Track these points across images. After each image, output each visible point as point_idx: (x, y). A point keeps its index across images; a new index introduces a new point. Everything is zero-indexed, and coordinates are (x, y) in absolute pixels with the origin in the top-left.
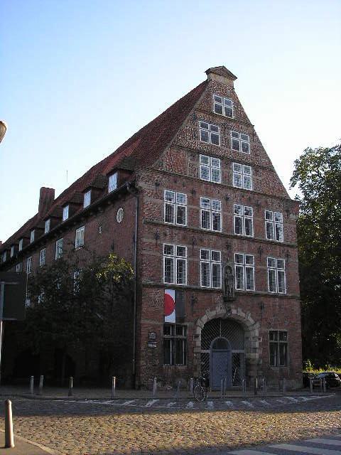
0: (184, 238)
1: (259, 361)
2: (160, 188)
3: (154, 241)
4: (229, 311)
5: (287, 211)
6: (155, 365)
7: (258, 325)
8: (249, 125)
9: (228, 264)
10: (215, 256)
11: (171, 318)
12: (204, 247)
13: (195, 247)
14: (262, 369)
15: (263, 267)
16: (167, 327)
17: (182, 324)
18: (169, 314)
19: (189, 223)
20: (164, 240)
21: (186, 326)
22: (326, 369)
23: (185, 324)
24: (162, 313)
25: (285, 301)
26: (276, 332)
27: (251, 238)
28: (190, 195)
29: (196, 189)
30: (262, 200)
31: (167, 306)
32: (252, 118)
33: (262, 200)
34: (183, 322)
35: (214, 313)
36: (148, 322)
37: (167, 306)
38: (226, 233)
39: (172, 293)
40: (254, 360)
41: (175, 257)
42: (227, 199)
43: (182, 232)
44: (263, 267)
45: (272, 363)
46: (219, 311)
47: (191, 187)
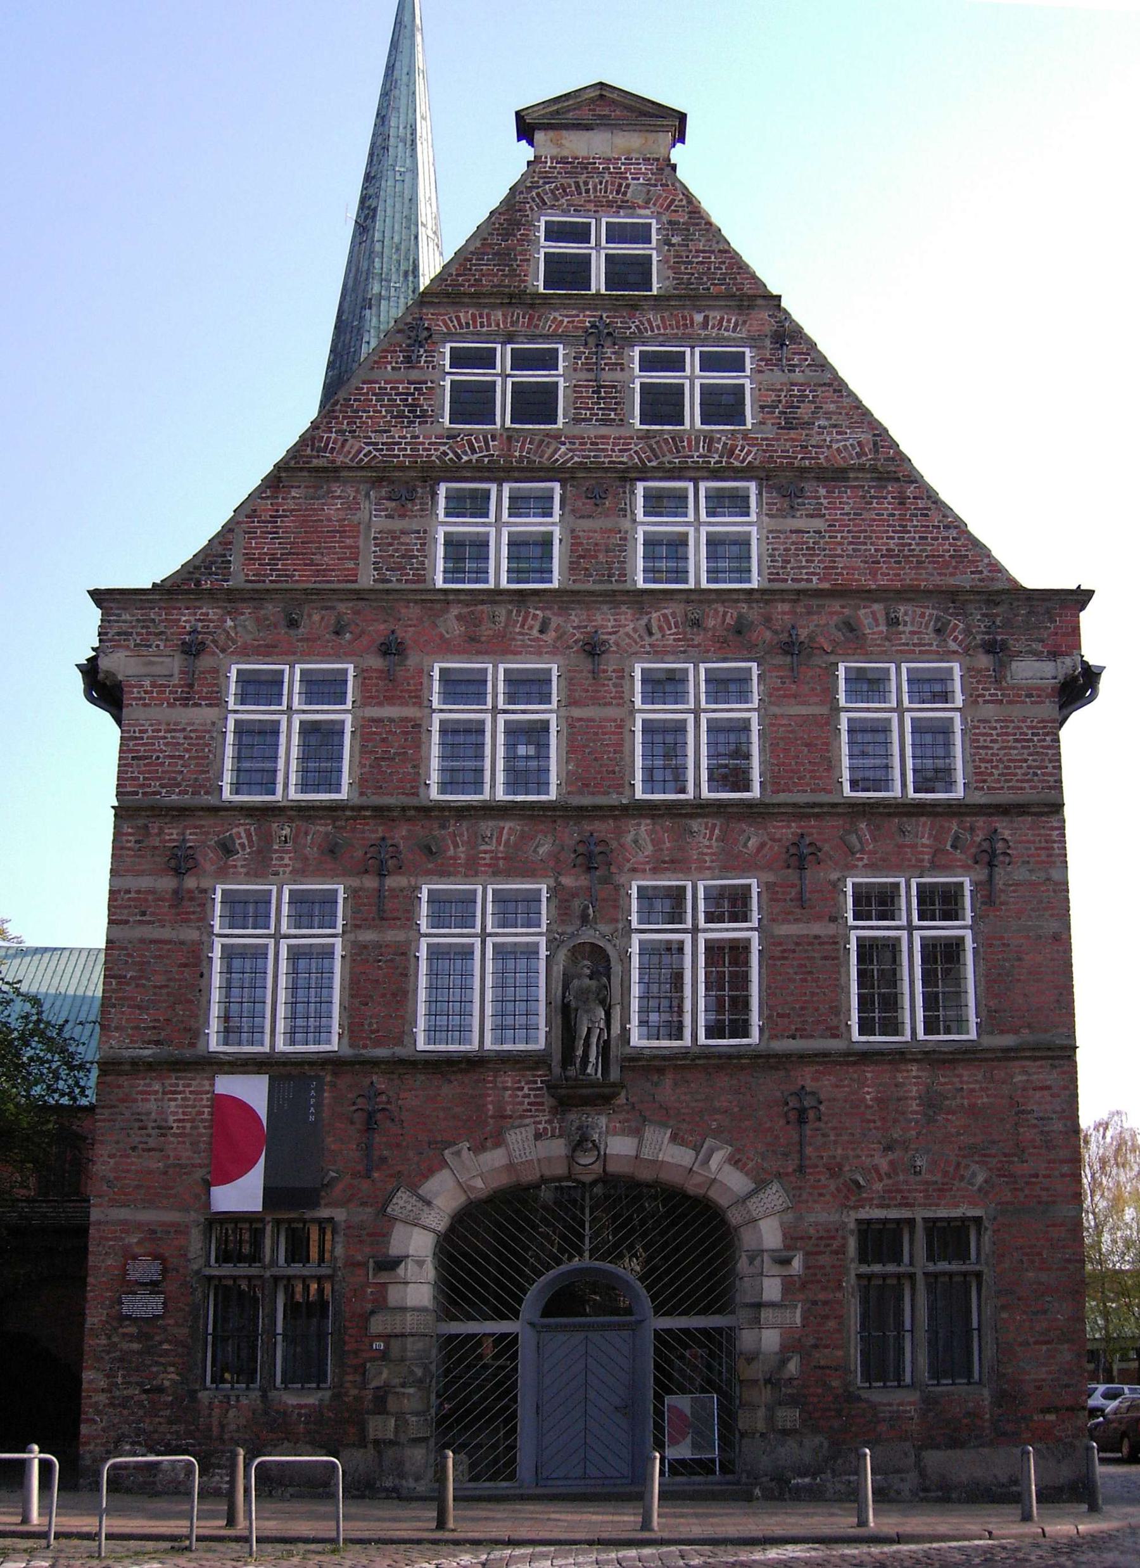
0: (332, 850)
1: (784, 1362)
2: (205, 662)
3: (167, 883)
4: (581, 1142)
5: (991, 648)
6: (160, 1390)
7: (774, 1196)
8: (751, 298)
9: (588, 936)
10: (939, 903)
11: (242, 1194)
12: (443, 873)
13: (391, 882)
14: (793, 1401)
15: (819, 929)
16: (234, 1235)
17: (309, 1215)
18: (227, 1176)
19: (362, 783)
20: (223, 873)
21: (323, 1224)
22: (869, 1554)
23: (324, 1213)
24: (200, 1173)
25: (969, 1077)
26: (911, 1222)
27: (749, 805)
28: (375, 662)
29: (407, 634)
30: (818, 625)
31: (230, 1140)
32: (772, 275)
33: (818, 625)
34: (315, 1205)
35: (495, 1158)
36: (123, 1214)
37: (230, 1140)
38: (576, 801)
39: (253, 1092)
40: (752, 1358)
41: (910, 934)
42: (593, 649)
43: (322, 828)
44: (819, 929)
45: (881, 1364)
46: (529, 1149)
47: (379, 629)
